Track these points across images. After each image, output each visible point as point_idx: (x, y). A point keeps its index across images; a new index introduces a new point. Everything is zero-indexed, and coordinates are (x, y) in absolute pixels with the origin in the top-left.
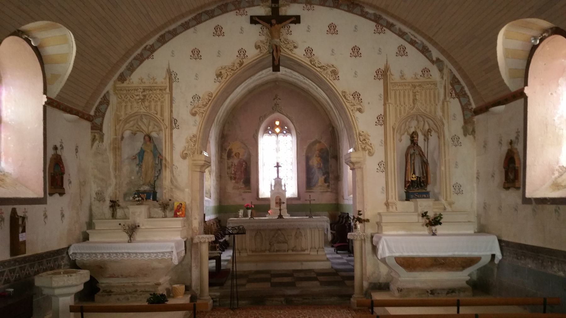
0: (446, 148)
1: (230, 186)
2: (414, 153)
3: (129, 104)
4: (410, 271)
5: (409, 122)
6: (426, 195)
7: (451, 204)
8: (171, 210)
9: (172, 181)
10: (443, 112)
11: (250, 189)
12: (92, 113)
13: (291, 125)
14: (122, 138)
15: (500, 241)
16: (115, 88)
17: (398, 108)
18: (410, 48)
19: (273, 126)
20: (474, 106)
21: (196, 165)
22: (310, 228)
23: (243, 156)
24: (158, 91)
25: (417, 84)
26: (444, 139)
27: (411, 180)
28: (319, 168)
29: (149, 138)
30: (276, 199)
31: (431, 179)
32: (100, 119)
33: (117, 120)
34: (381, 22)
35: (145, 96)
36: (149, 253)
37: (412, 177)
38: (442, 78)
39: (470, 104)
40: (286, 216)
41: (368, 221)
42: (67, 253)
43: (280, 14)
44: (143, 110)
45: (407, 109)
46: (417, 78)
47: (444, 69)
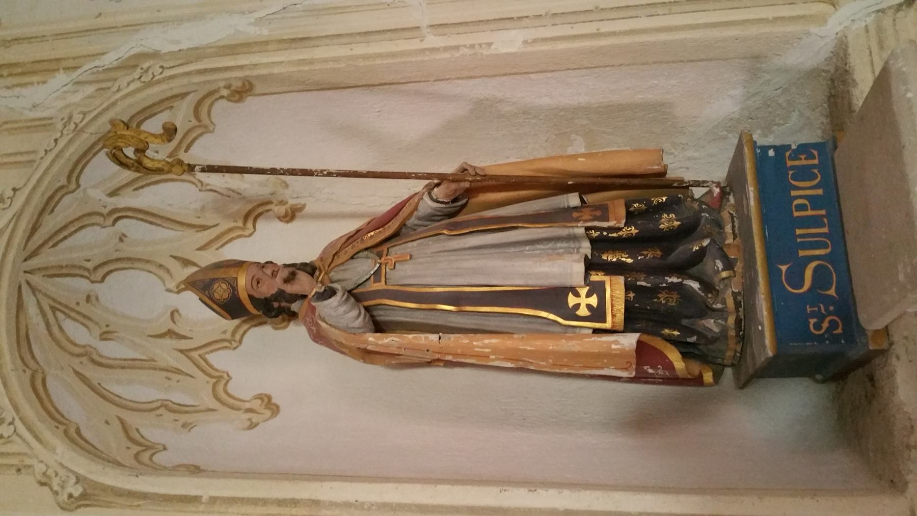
2: (355, 295)
5: (105, 336)
26: (262, 45)
27: (631, 321)
37: (598, 314)
47: (899, 372)
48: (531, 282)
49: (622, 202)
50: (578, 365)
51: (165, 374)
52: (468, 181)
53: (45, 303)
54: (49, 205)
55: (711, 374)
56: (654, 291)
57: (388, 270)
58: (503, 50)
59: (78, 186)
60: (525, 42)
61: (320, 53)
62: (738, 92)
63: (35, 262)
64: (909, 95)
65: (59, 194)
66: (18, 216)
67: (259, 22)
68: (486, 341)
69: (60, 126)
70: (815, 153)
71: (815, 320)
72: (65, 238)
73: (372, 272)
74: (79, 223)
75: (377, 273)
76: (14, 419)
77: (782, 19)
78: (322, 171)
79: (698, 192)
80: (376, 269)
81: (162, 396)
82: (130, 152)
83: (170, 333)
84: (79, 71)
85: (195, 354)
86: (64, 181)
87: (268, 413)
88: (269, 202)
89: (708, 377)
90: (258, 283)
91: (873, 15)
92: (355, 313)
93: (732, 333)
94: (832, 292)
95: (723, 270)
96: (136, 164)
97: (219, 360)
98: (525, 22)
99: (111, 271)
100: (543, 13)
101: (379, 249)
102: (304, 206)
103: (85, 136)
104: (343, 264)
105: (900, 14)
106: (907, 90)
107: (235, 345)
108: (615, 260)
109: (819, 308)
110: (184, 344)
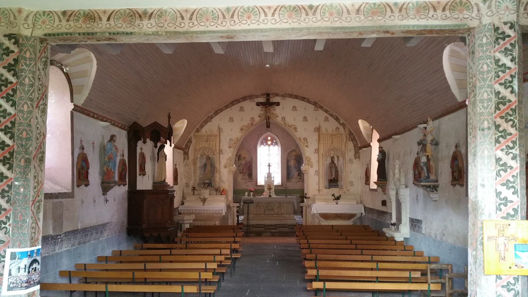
0: (346, 164)
1: (240, 177)
3: (201, 143)
4: (326, 220)
6: (337, 186)
7: (348, 190)
8: (219, 192)
9: (220, 178)
10: (345, 147)
11: (252, 179)
12: (184, 147)
13: (278, 140)
14: (197, 158)
15: (365, 207)
16: (194, 135)
17: (325, 146)
18: (330, 117)
19: (266, 140)
20: (359, 145)
21: (230, 171)
22: (286, 203)
23: (248, 159)
24: (214, 137)
25: (334, 134)
28: (295, 167)
29: (208, 158)
30: (268, 186)
31: (340, 179)
32: (188, 149)
33: (195, 150)
34: (317, 105)
35: (208, 139)
36: (213, 210)
38: (345, 132)
39: (358, 144)
40: (274, 196)
41: (309, 198)
42: (178, 210)
43: (270, 101)
44: (207, 145)
45: (329, 146)
46: (333, 132)
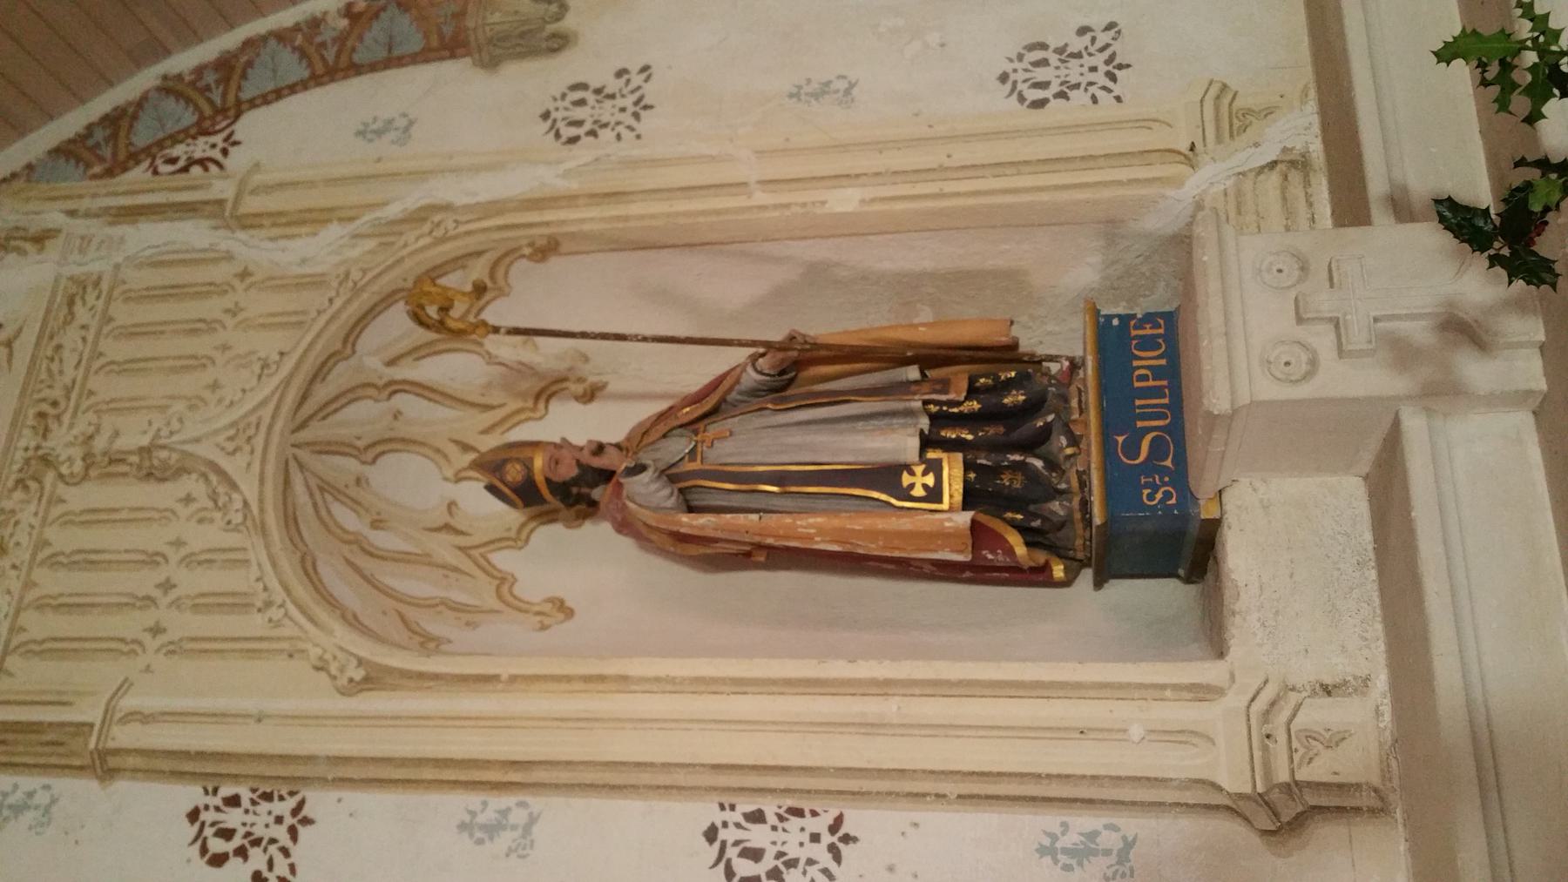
2: (670, 475)
5: (377, 524)
26: (571, 199)
27: (970, 499)
37: (934, 494)
48: (862, 459)
49: (967, 376)
50: (910, 548)
51: (441, 571)
52: (795, 349)
53: (313, 482)
54: (320, 373)
55: (1062, 567)
56: (996, 470)
57: (705, 448)
58: (839, 209)
59: (354, 352)
60: (863, 201)
61: (635, 209)
62: (1095, 259)
63: (304, 435)
64: (1205, 258)
65: (332, 361)
66: (287, 382)
67: (567, 174)
68: (811, 520)
69: (335, 284)
70: (1162, 322)
71: (1149, 491)
72: (336, 411)
73: (687, 451)
74: (350, 395)
75: (693, 452)
76: (284, 601)
77: (1137, 181)
78: (636, 336)
79: (1054, 368)
80: (691, 446)
81: (443, 594)
82: (432, 311)
83: (447, 528)
84: (358, 223)
85: (475, 553)
86: (338, 346)
87: (561, 616)
88: (565, 379)
89: (1058, 571)
90: (557, 463)
91: (1233, 178)
92: (666, 492)
93: (1078, 516)
94: (1168, 463)
95: (1068, 446)
96: (437, 324)
97: (503, 560)
98: (863, 180)
99: (383, 453)
100: (883, 171)
101: (696, 426)
102: (604, 386)
103: (365, 296)
104: (653, 443)
105: (1262, 177)
106: (1204, 254)
107: (520, 543)
108: (954, 436)
109: (1154, 479)
110: (461, 541)
